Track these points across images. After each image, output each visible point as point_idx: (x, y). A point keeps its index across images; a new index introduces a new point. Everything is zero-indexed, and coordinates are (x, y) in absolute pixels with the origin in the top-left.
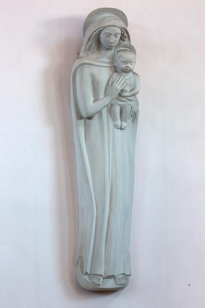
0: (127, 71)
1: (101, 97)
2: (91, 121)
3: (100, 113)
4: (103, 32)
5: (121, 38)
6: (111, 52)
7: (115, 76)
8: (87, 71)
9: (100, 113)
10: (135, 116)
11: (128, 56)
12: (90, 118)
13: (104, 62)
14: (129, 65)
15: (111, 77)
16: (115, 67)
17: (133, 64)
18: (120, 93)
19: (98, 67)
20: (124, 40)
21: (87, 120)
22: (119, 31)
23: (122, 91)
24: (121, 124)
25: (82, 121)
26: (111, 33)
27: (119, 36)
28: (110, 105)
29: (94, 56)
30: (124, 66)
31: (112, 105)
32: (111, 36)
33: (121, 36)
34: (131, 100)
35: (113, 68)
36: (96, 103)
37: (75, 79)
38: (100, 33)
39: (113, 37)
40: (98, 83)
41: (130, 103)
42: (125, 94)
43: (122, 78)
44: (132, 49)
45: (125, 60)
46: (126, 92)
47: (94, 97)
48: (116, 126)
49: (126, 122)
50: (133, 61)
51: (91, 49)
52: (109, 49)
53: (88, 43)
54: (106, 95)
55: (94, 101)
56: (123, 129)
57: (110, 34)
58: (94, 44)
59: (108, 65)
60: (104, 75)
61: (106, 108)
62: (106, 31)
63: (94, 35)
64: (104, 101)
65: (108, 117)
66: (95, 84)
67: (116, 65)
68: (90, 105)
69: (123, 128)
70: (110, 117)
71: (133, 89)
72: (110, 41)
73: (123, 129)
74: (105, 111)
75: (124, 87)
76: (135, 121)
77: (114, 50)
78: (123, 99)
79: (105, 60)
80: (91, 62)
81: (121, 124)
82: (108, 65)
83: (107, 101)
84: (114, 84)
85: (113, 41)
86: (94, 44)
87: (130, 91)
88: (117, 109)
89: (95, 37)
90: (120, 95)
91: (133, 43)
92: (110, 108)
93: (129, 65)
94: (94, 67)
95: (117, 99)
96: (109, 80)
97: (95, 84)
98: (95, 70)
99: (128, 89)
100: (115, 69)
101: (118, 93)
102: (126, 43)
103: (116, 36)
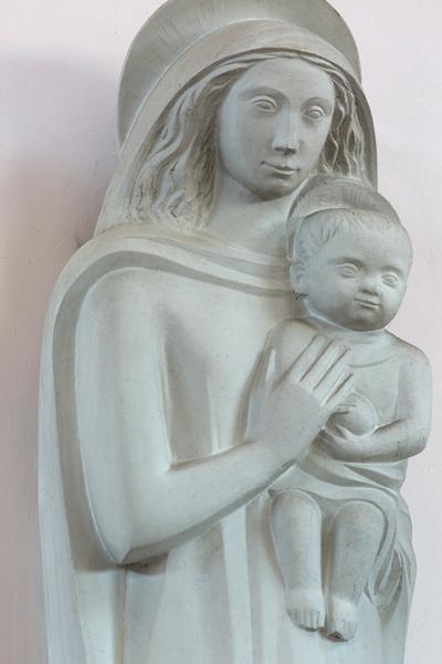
0: (362, 318)
1: (216, 451)
2: (152, 580)
3: (206, 531)
4: (238, 87)
5: (329, 145)
6: (273, 218)
7: (298, 340)
8: (141, 299)
9: (206, 531)
10: (393, 587)
11: (369, 231)
12: (146, 561)
13: (233, 263)
14: (376, 281)
15: (273, 342)
16: (296, 298)
17: (399, 283)
18: (322, 433)
19: (201, 284)
20: (342, 165)
21: (132, 579)
22: (324, 89)
23: (337, 419)
24: (330, 608)
25: (105, 579)
26: (283, 90)
27: (325, 124)
28: (264, 497)
29: (184, 226)
30: (349, 286)
31: (276, 498)
32: (284, 112)
33: (333, 133)
34: (383, 481)
35: (282, 302)
36: (186, 474)
37: (70, 359)
38: (223, 94)
39: (294, 116)
40: (203, 367)
41: (377, 494)
42: (351, 441)
43: (332, 354)
44: (380, 207)
45: (356, 255)
46: (357, 431)
47: (174, 445)
48: (295, 615)
49: (354, 598)
50: (399, 263)
51: (167, 184)
52: (266, 195)
53: (147, 151)
54: (242, 438)
55: (176, 467)
56: (336, 637)
57: (280, 99)
58: (183, 160)
59: (258, 282)
60: (234, 330)
61: (242, 511)
62: (253, 79)
63: (186, 102)
64: (234, 469)
65: (251, 562)
66: (184, 371)
67: (298, 287)
68: (159, 485)
69: (339, 627)
70: (264, 564)
71: (396, 422)
72: (279, 142)
73: (336, 637)
74: (235, 529)
75: (351, 401)
76: (396, 614)
77: (289, 201)
78: (341, 469)
79: (240, 250)
80: (164, 252)
81: (330, 608)
82: (258, 282)
83: (251, 468)
84: (295, 377)
85: (292, 143)
86: (183, 160)
87: (382, 429)
88: (309, 524)
89: (192, 114)
90: (323, 443)
91: (384, 188)
92: (268, 512)
93: (376, 281)
94: (181, 279)
95: (307, 466)
96: (262, 361)
97: (184, 371)
98: (187, 298)
99: (366, 413)
100: (294, 307)
101: (314, 434)
102: (354, 179)
103: (309, 113)
